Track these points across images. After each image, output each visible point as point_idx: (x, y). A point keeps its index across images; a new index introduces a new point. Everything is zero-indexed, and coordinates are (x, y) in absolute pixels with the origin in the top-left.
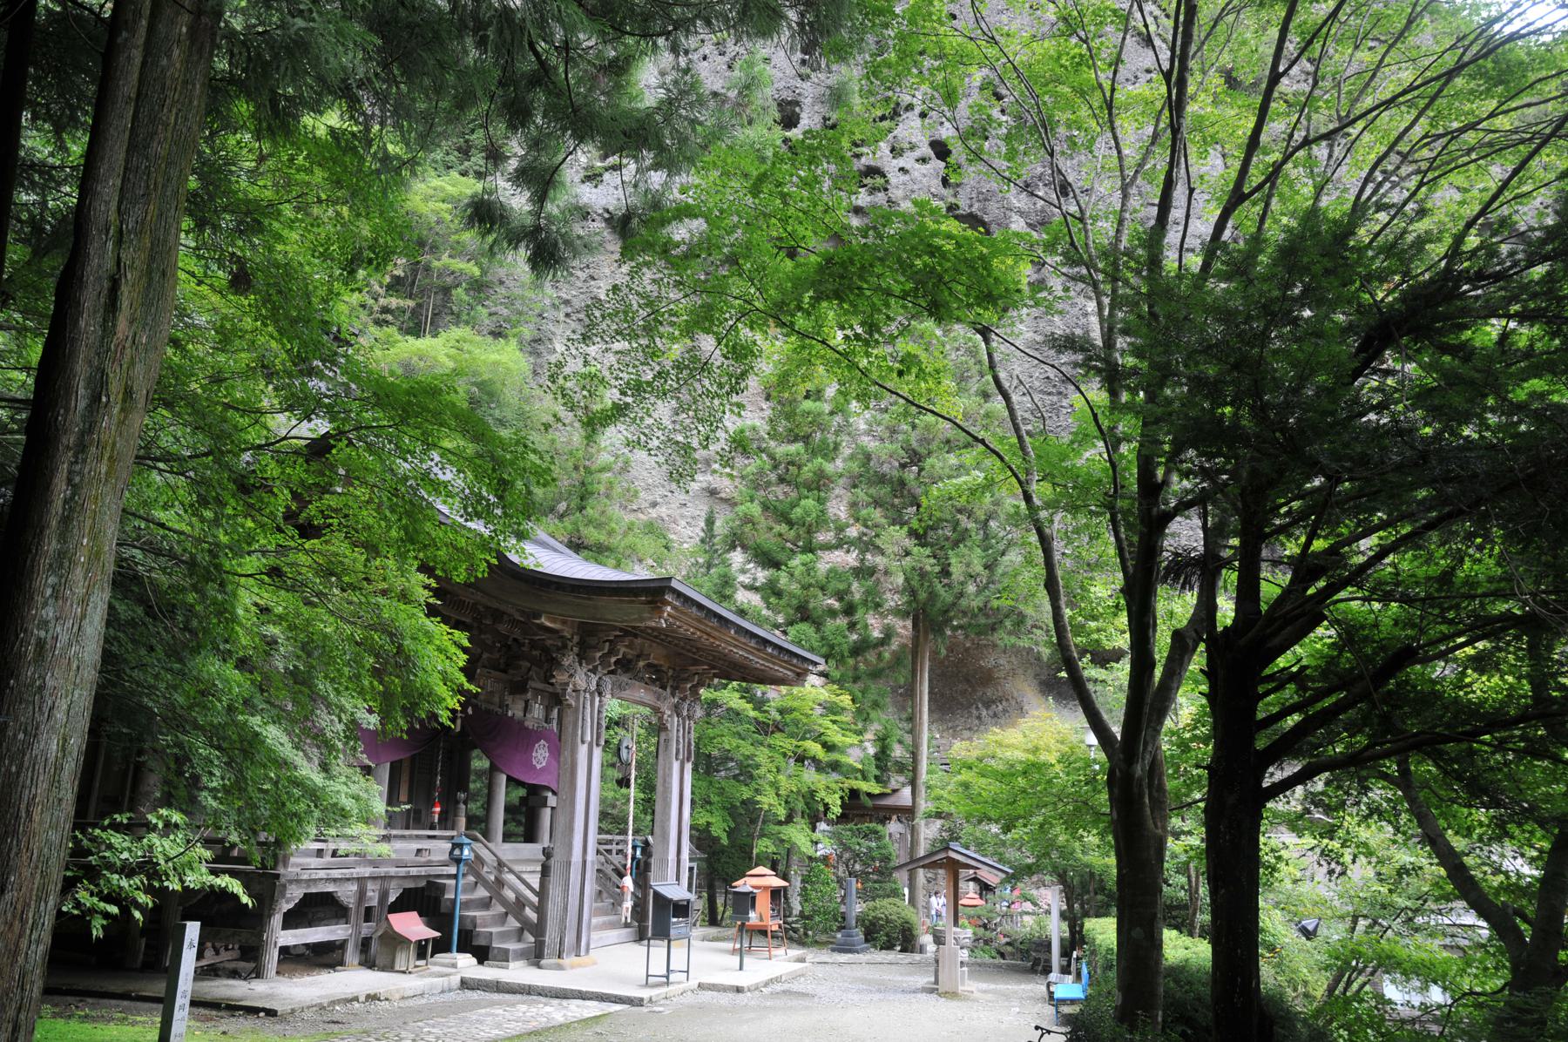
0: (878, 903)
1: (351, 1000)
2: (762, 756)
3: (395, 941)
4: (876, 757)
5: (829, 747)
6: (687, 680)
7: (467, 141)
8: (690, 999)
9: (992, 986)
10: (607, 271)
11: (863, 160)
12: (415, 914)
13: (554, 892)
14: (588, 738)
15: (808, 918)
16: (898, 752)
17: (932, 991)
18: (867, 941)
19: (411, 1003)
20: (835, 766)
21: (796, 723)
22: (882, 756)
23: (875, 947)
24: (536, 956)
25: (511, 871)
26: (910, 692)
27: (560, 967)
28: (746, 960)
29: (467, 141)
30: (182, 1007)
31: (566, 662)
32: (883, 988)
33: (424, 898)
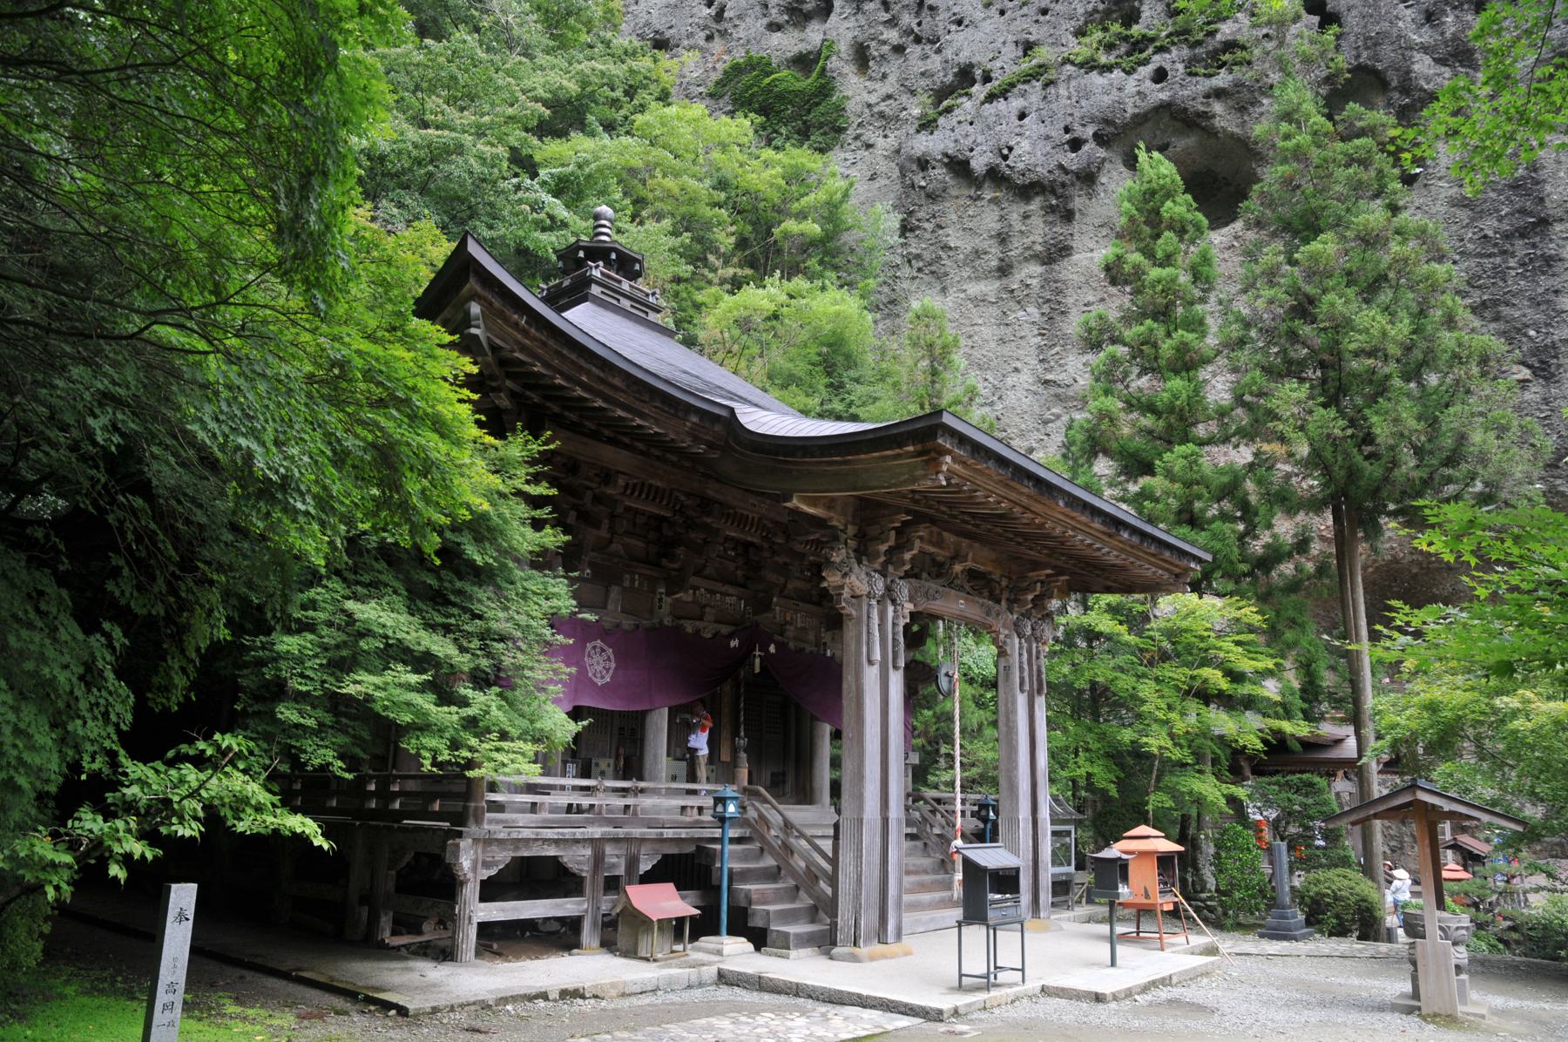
0: (1321, 874)
1: (537, 996)
2: (1147, 690)
3: (639, 922)
4: (1303, 690)
5: (1236, 677)
6: (1027, 590)
7: (805, 123)
8: (1022, 1011)
9: (1513, 1003)
10: (954, 217)
11: (1219, 37)
12: (671, 886)
13: (846, 858)
14: (877, 656)
15: (1224, 893)
16: (1328, 680)
17: (1410, 1011)
18: (1308, 923)
19: (635, 1001)
20: (1249, 703)
21: (1189, 648)
22: (1310, 691)
23: (1321, 932)
24: (826, 942)
25: (802, 835)
26: (1342, 599)
27: (854, 959)
28: (1121, 950)
29: (805, 123)
30: (168, 1007)
31: (836, 558)
32: (1330, 1001)
33: (687, 867)
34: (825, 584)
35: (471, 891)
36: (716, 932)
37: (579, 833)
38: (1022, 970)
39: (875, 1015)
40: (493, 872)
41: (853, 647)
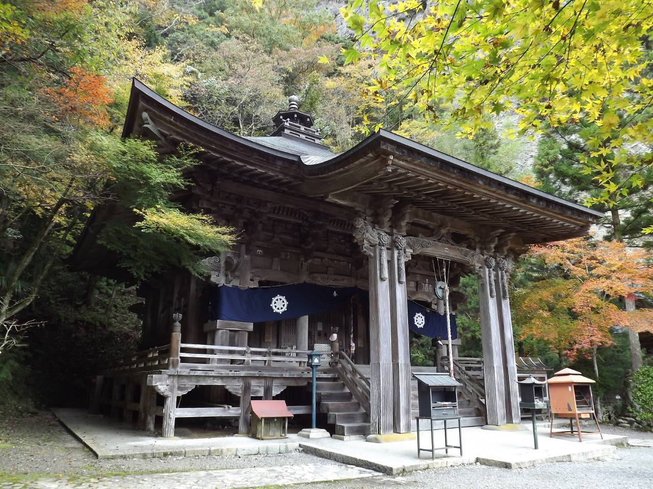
14: (386, 274)
24: (363, 432)
27: (377, 441)
34: (355, 241)
35: (171, 403)
36: (310, 427)
37: (237, 374)
38: (460, 448)
39: (357, 469)
40: (185, 393)
41: (373, 273)
